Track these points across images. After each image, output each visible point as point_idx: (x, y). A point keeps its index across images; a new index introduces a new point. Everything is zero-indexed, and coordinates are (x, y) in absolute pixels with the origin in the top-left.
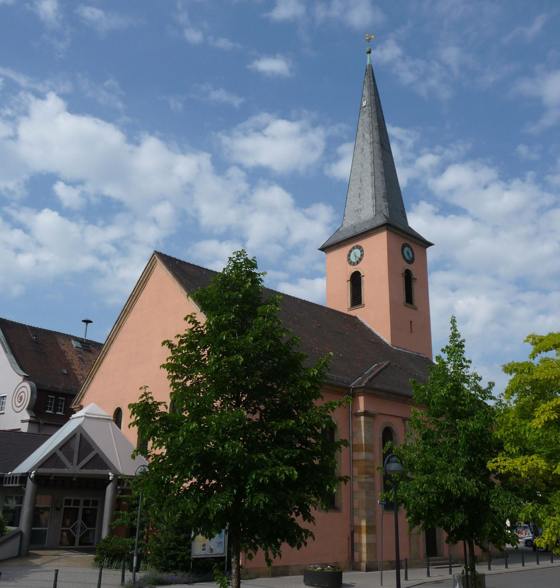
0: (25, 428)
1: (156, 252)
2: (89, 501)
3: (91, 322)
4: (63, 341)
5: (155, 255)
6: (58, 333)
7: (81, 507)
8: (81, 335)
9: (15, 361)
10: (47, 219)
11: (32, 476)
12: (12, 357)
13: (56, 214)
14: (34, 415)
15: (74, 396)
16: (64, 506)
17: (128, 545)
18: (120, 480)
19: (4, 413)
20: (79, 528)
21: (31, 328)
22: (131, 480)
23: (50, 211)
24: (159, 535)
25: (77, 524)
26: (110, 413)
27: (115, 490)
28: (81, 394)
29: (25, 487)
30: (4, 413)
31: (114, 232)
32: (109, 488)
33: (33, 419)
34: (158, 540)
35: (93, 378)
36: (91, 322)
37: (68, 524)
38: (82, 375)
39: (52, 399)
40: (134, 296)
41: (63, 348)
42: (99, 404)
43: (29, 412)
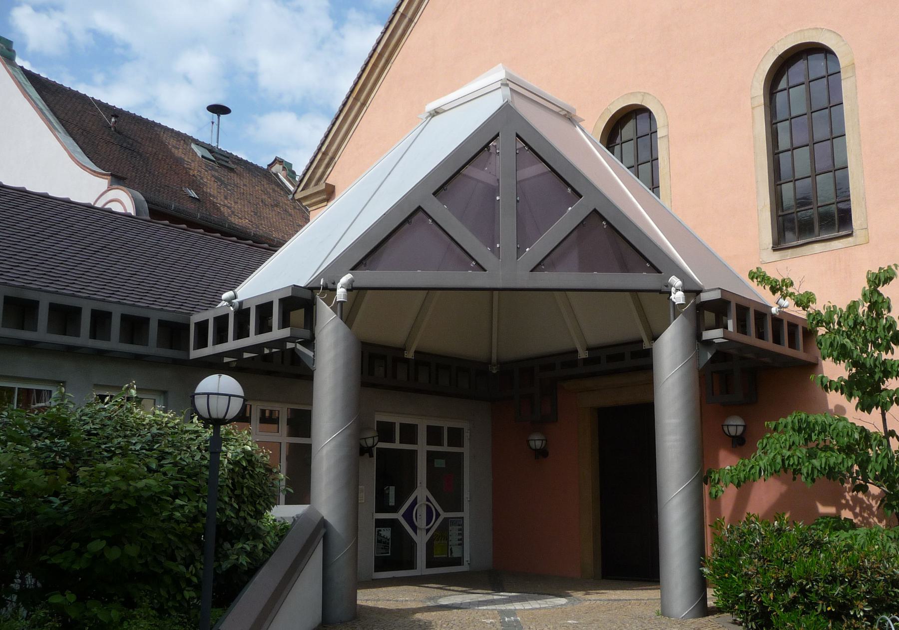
7: (422, 448)
11: (341, 293)
12: (70, 140)
19: (801, 76)
20: (423, 512)
25: (415, 502)
29: (310, 343)
35: (364, 104)
37: (392, 502)
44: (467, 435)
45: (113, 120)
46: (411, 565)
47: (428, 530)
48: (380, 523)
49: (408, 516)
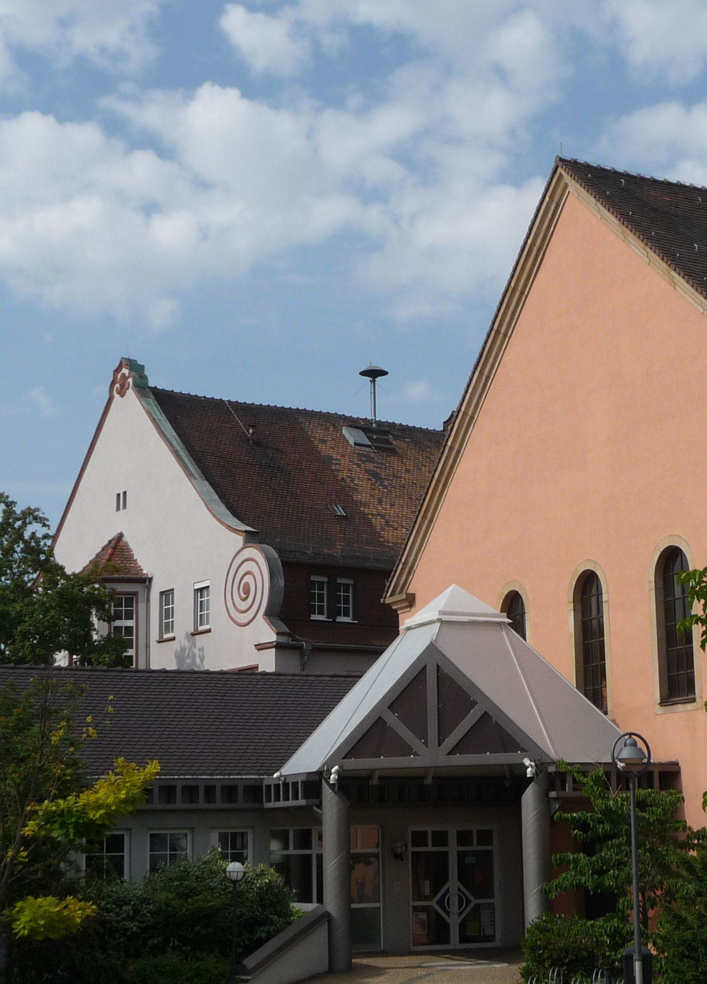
0: (267, 662)
1: (561, 160)
2: (425, 834)
3: (383, 373)
4: (319, 433)
5: (560, 170)
6: (304, 413)
7: (453, 849)
8: (361, 411)
9: (216, 497)
10: (213, 116)
11: (333, 777)
13: (232, 94)
14: (286, 630)
15: (387, 574)
16: (411, 849)
17: (601, 935)
18: (555, 777)
19: (209, 631)
21: (236, 405)
22: (585, 774)
23: (217, 88)
24: (678, 907)
25: (448, 891)
26: (490, 608)
27: (545, 801)
28: (405, 564)
29: (320, 806)
30: (209, 631)
31: (392, 123)
32: (529, 799)
33: (284, 639)
34: (680, 921)
36: (383, 373)
37: (427, 892)
38: (382, 516)
39: (321, 584)
40: (515, 289)
41: (324, 450)
42: (467, 584)
43: (272, 624)
44: (495, 835)
45: (251, 431)
46: (446, 941)
47: (460, 914)
48: (416, 909)
49: (441, 903)
